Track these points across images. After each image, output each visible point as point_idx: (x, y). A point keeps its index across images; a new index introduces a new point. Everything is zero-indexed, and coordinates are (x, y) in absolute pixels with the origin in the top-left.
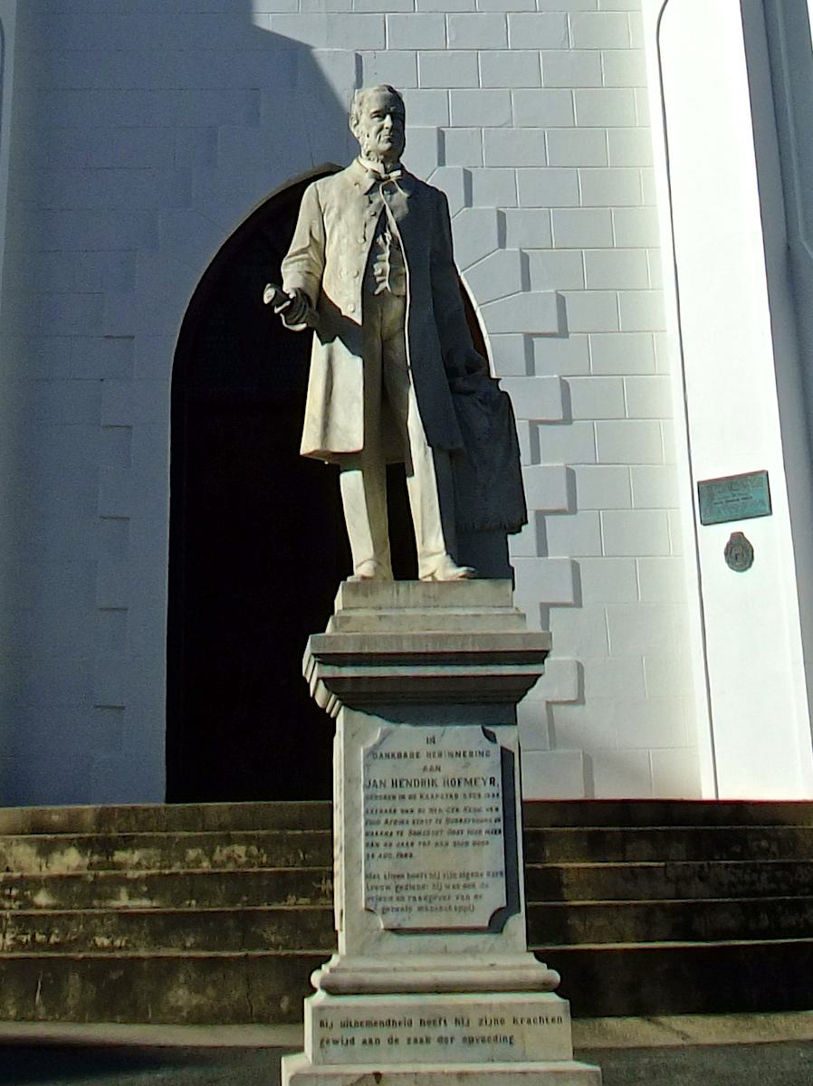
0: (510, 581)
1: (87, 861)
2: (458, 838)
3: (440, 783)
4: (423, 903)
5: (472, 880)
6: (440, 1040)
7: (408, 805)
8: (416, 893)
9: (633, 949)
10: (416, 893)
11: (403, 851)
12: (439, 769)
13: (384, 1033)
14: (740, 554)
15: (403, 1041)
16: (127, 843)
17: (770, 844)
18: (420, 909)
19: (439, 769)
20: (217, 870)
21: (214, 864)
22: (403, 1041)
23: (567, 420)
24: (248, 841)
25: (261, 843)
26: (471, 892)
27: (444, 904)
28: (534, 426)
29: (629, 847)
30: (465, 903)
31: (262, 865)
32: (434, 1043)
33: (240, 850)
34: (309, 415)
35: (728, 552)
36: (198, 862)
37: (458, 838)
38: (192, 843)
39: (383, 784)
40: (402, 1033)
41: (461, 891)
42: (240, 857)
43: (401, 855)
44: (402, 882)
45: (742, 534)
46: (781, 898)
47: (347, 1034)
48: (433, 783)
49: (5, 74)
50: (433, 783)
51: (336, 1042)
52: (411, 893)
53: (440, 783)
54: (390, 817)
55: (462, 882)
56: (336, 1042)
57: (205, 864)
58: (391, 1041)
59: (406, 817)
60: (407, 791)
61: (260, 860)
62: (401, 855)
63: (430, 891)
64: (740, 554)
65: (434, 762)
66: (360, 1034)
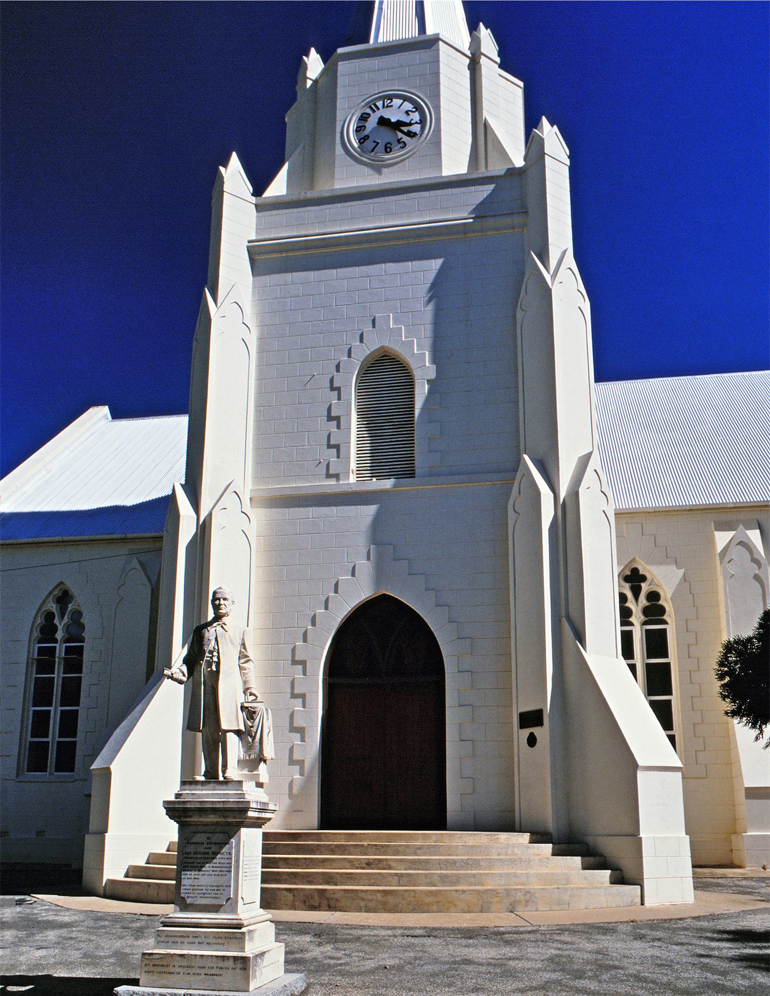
2: (216, 873)
3: (210, 853)
4: (201, 895)
5: (220, 888)
6: (199, 943)
7: (198, 861)
8: (200, 892)
10: (200, 892)
11: (196, 877)
12: (211, 848)
13: (179, 940)
14: (532, 741)
15: (186, 942)
18: (200, 897)
19: (211, 848)
20: (178, 800)
22: (186, 942)
26: (219, 892)
27: (209, 896)
30: (217, 896)
32: (197, 944)
34: (593, 873)
35: (528, 740)
37: (216, 873)
39: (190, 853)
40: (186, 940)
41: (216, 892)
43: (195, 878)
44: (195, 888)
47: (167, 939)
48: (208, 853)
50: (208, 853)
51: (163, 942)
52: (198, 891)
53: (210, 853)
54: (192, 865)
55: (216, 888)
56: (163, 942)
58: (181, 943)
59: (198, 971)
60: (199, 856)
62: (195, 878)
63: (204, 891)
64: (532, 741)
65: (209, 846)
66: (171, 939)
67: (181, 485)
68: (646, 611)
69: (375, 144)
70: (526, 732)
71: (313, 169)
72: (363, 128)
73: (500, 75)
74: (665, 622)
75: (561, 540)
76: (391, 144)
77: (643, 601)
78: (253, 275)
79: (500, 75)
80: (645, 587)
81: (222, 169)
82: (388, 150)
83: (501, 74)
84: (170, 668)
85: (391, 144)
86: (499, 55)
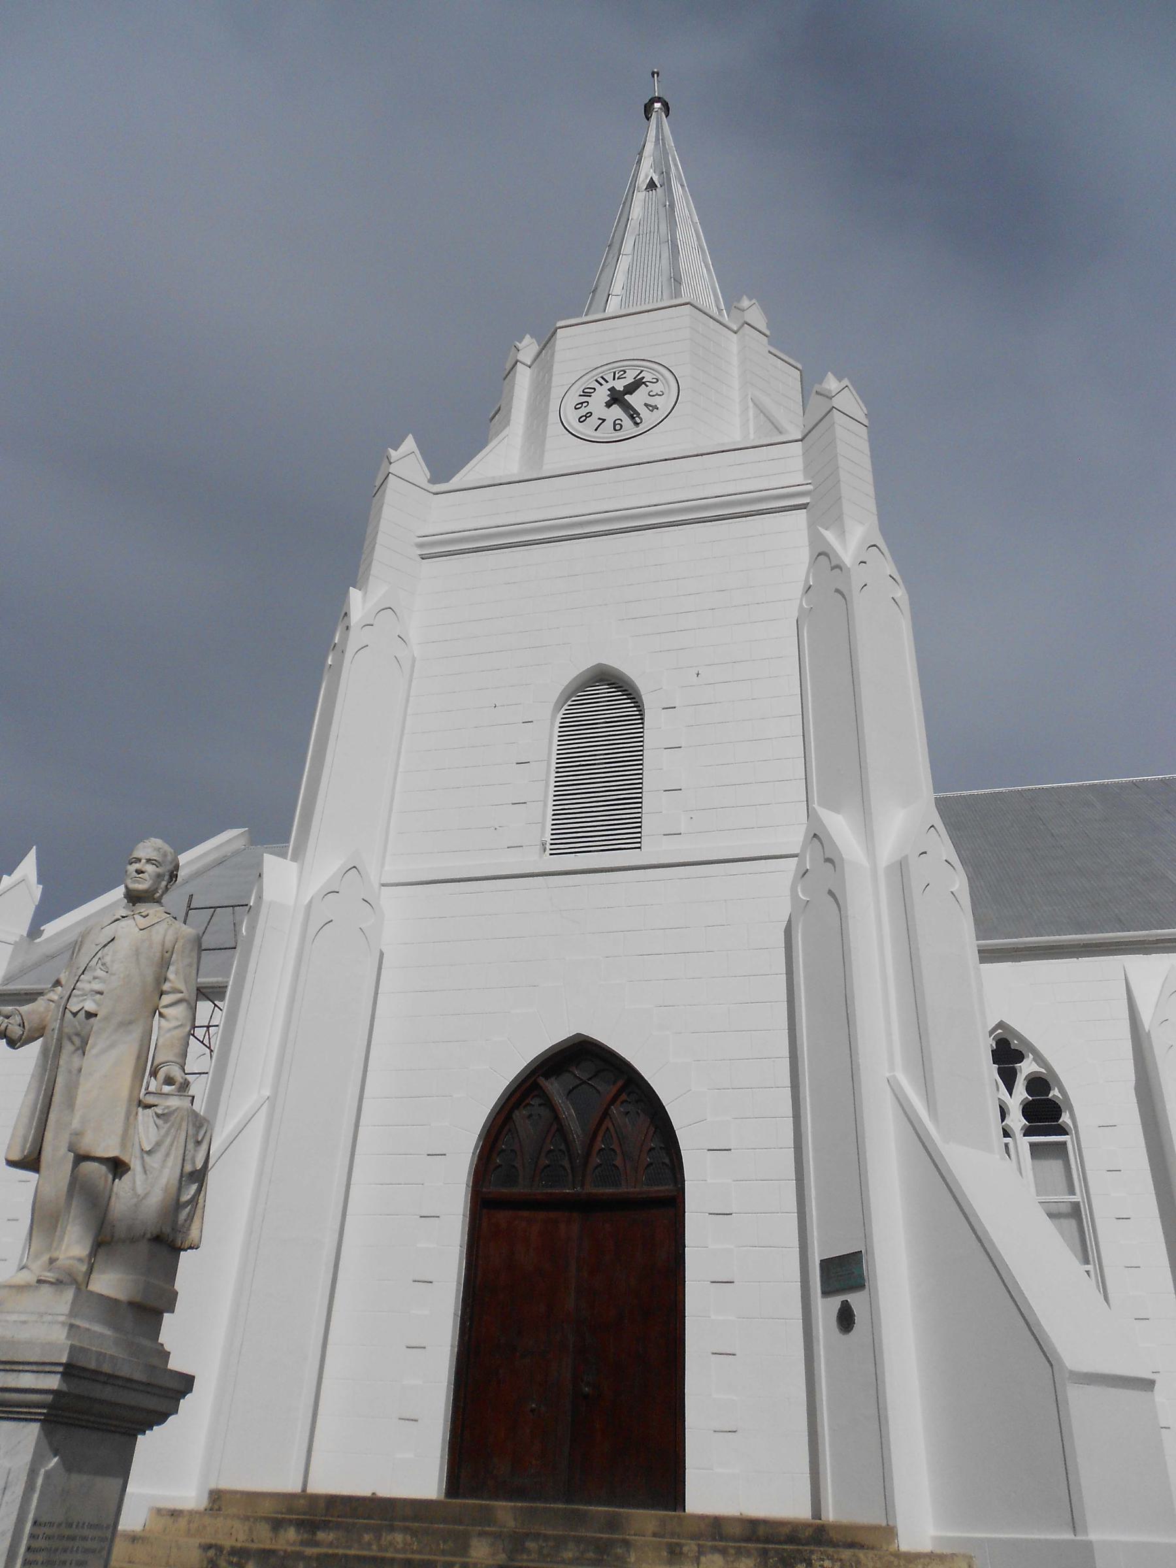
0: (121, 1481)
1: (300, 1537)
9: (922, 686)
16: (325, 1525)
17: (833, 1564)
21: (381, 1549)
23: (834, 407)
24: (406, 1530)
25: (414, 1533)
28: (645, 157)
29: (703, 1559)
31: (413, 1552)
33: (399, 1538)
36: (369, 1544)
38: (367, 1529)
42: (397, 1543)
45: (177, 1293)
46: (816, 799)
49: (458, 475)
57: (374, 1547)
61: (411, 1547)
67: (120, 1180)
68: (1028, 1111)
69: (601, 421)
70: (836, 1302)
71: (32, 1313)
72: (585, 404)
73: (770, 352)
74: (1062, 1131)
75: (1077, 1154)
76: (621, 420)
77: (1021, 1093)
78: (1032, 1159)
79: (770, 352)
80: (1027, 1067)
81: (391, 451)
82: (618, 427)
83: (771, 351)
84: (520, 343)
85: (621, 420)
86: (768, 327)
